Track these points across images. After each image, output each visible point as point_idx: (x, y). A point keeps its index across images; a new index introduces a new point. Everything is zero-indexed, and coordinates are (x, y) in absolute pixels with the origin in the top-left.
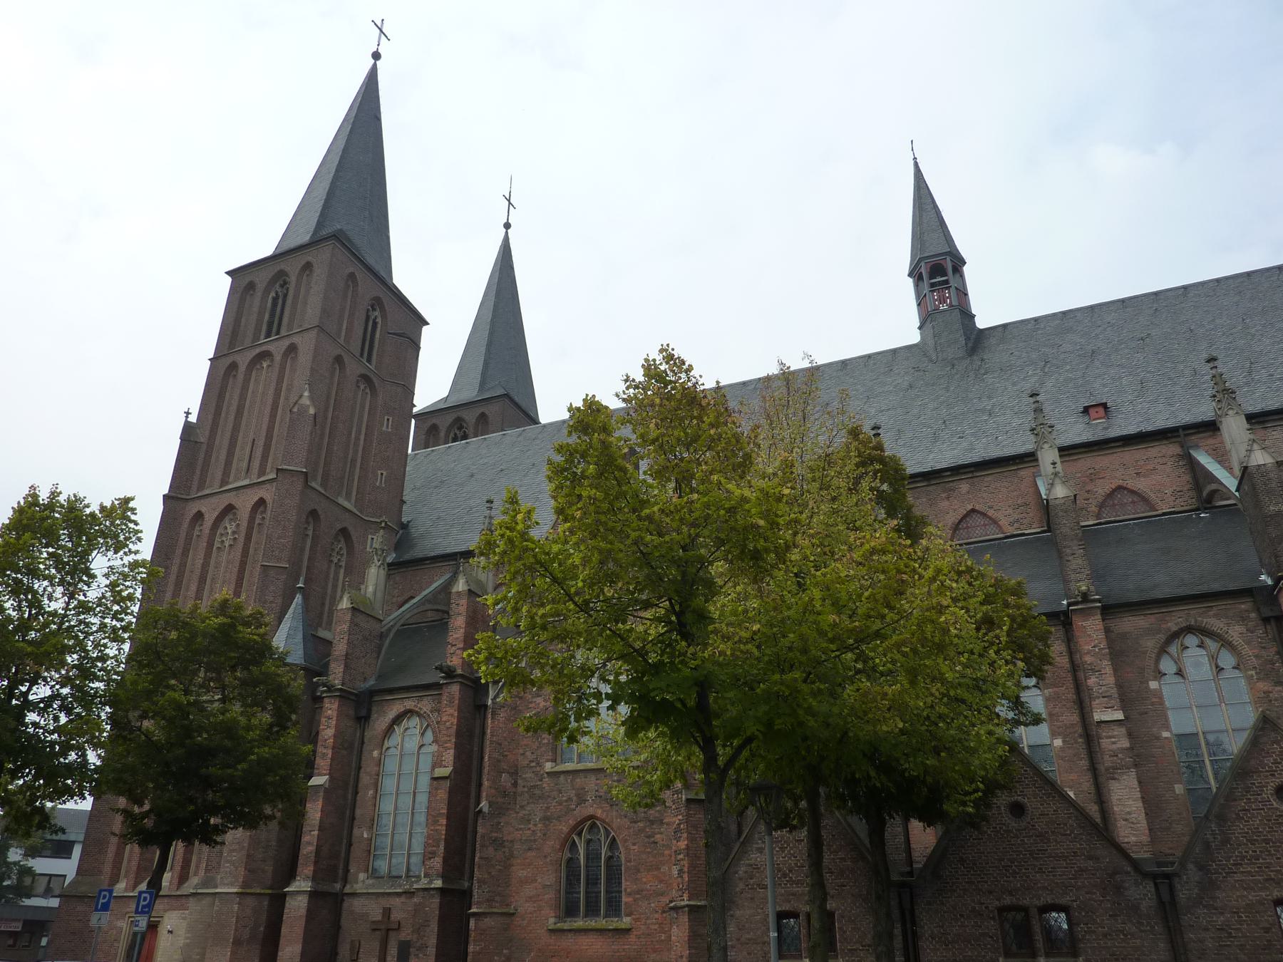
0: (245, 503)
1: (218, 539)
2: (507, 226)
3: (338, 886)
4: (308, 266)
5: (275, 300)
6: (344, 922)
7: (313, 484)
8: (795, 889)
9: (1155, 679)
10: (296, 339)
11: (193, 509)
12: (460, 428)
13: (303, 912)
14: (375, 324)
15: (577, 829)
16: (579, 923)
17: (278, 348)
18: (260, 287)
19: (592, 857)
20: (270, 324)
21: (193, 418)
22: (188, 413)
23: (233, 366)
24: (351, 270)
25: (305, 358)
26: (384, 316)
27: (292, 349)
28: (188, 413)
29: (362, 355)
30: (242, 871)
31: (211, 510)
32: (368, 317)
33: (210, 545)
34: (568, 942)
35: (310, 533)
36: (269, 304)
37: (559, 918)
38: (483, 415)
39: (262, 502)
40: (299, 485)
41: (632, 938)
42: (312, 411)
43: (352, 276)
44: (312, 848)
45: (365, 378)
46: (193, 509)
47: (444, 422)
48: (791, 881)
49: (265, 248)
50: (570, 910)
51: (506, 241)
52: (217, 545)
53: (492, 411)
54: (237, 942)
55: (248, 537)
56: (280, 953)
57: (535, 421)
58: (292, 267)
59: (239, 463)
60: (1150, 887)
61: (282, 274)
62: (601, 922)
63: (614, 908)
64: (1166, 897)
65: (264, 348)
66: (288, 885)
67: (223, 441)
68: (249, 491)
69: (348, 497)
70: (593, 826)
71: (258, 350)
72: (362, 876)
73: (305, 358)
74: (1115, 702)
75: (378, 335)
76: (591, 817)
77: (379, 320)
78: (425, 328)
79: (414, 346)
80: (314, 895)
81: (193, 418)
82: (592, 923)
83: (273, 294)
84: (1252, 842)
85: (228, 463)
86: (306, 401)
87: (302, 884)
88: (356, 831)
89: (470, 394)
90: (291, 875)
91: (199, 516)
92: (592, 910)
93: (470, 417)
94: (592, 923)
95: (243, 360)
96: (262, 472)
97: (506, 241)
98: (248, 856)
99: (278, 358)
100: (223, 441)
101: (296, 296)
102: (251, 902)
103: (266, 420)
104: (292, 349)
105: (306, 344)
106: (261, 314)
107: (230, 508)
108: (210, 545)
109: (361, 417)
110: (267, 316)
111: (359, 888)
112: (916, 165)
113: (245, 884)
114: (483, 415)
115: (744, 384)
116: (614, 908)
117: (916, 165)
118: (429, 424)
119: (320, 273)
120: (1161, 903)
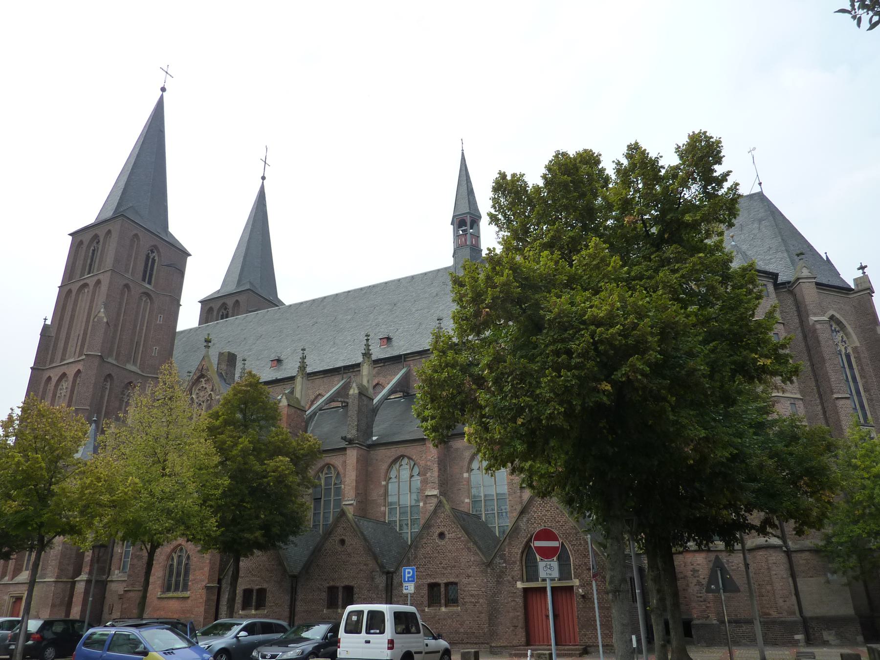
0: (71, 372)
1: (59, 392)
2: (263, 178)
3: (105, 577)
4: (109, 232)
5: (94, 251)
6: (107, 595)
7: (110, 360)
8: (255, 579)
9: (467, 472)
10: (101, 277)
11: (46, 375)
12: (226, 309)
13: (83, 590)
14: (154, 260)
15: (174, 550)
16: (170, 595)
17: (92, 282)
18: (86, 243)
19: (180, 563)
20: (90, 265)
21: (49, 322)
22: (45, 319)
23: (70, 291)
24: (135, 232)
25: (104, 287)
26: (159, 256)
27: (99, 282)
28: (45, 319)
29: (144, 280)
30: (56, 570)
31: (55, 375)
32: (148, 257)
33: (54, 395)
34: (165, 602)
35: (108, 387)
36: (90, 254)
37: (163, 592)
38: (237, 301)
39: (79, 371)
40: (97, 362)
41: (189, 601)
42: (105, 320)
43: (136, 235)
44: (89, 558)
45: (147, 294)
46: (46, 375)
47: (216, 306)
48: (253, 575)
49: (90, 219)
50: (168, 589)
51: (262, 187)
52: (58, 395)
53: (242, 298)
54: (53, 606)
55: (72, 392)
56: (675, 563)
57: (273, 301)
58: (101, 232)
59: (71, 349)
60: (384, 577)
61: (96, 237)
62: (179, 594)
63: (186, 588)
64: (389, 583)
65: (85, 281)
66: (78, 576)
67: (63, 335)
68: (73, 365)
69: (134, 363)
70: (182, 549)
71: (82, 283)
72: (117, 572)
73: (104, 287)
74: (436, 486)
75: (155, 267)
76: (180, 545)
77: (156, 258)
78: (189, 258)
79: (180, 273)
80: (88, 582)
81: (49, 322)
82: (175, 595)
83: (92, 248)
84: (425, 558)
85: (65, 349)
86: (102, 314)
87: (84, 577)
88: (115, 549)
89: (232, 288)
90: (78, 573)
91: (49, 378)
92: (177, 589)
93: (230, 302)
94: (175, 595)
95: (75, 287)
96: (80, 354)
97: (262, 187)
98: (60, 562)
99: (91, 288)
100: (63, 335)
101: (103, 251)
102: (60, 585)
103: (84, 324)
104: (99, 282)
105: (105, 279)
106: (85, 260)
107: (64, 375)
108: (54, 395)
109: (144, 316)
110: (89, 261)
111: (114, 578)
112: (463, 154)
113: (58, 577)
114: (237, 301)
115: (361, 289)
116: (186, 588)
117: (463, 154)
118: (208, 307)
119: (115, 236)
120: (387, 584)
